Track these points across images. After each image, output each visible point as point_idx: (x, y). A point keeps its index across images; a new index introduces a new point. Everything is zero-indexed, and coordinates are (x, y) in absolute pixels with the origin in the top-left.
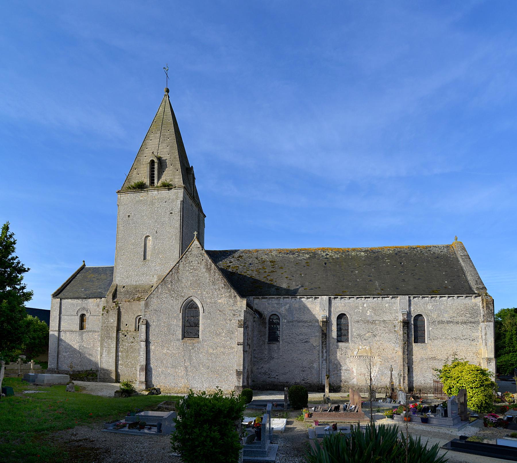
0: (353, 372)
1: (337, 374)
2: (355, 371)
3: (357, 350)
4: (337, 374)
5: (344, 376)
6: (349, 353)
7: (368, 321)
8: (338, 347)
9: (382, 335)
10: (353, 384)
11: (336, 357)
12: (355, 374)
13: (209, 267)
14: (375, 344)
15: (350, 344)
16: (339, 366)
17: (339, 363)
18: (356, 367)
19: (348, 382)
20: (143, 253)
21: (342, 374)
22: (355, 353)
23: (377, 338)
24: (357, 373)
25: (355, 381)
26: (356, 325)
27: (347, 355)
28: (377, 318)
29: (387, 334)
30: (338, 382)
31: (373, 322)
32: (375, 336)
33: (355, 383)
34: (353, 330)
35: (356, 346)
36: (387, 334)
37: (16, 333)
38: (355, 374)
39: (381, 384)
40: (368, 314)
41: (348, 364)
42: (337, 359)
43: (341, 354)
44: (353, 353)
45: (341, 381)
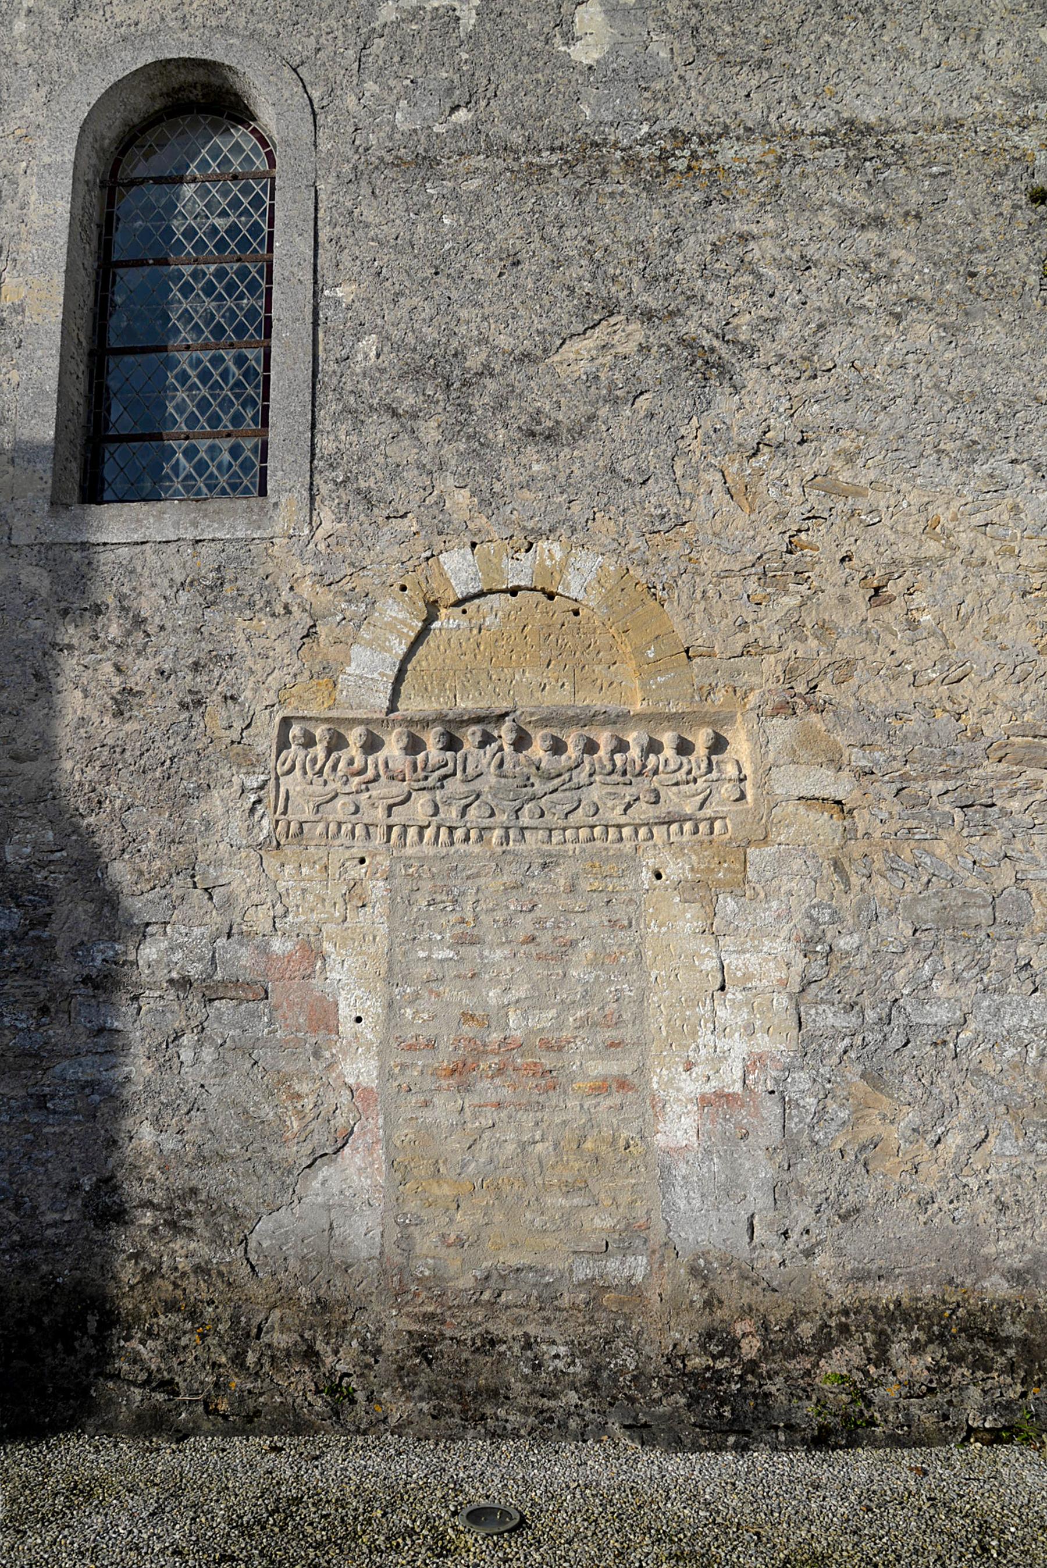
0: (324, 1017)
1: (36, 1057)
2: (351, 988)
3: (399, 616)
4: (36, 1057)
5: (173, 1096)
6: (266, 677)
7: (587, 154)
8: (73, 584)
9: (836, 346)
10: (328, 1256)
11: (45, 748)
12: (360, 1069)
13: (876, 423)
14: (709, 504)
15: (286, 529)
16: (74, 914)
17: (88, 866)
18: (375, 920)
19: (231, 1222)
20: (320, 251)
21: (139, 1068)
22: (366, 670)
23: (754, 401)
24: (396, 1043)
25: (348, 1203)
26: (382, 215)
27: (217, 717)
28: (746, 97)
29: (923, 330)
30: (55, 1216)
31: (676, 160)
32: (708, 366)
33: (364, 1234)
34: (344, 277)
35: (388, 549)
36: (923, 330)
37: (484, 347)
38: (360, 1069)
39: (862, 1245)
40: (584, 54)
41: (237, 878)
42: (45, 798)
43: (123, 704)
44: (328, 674)
45: (108, 1210)
